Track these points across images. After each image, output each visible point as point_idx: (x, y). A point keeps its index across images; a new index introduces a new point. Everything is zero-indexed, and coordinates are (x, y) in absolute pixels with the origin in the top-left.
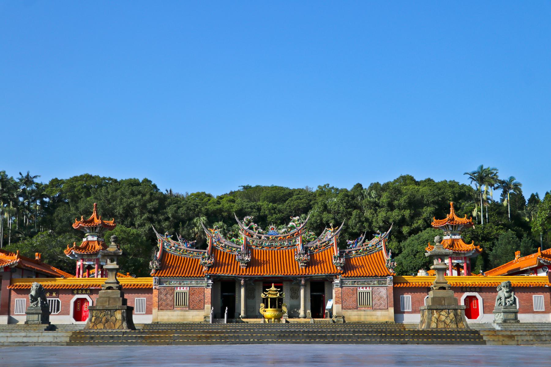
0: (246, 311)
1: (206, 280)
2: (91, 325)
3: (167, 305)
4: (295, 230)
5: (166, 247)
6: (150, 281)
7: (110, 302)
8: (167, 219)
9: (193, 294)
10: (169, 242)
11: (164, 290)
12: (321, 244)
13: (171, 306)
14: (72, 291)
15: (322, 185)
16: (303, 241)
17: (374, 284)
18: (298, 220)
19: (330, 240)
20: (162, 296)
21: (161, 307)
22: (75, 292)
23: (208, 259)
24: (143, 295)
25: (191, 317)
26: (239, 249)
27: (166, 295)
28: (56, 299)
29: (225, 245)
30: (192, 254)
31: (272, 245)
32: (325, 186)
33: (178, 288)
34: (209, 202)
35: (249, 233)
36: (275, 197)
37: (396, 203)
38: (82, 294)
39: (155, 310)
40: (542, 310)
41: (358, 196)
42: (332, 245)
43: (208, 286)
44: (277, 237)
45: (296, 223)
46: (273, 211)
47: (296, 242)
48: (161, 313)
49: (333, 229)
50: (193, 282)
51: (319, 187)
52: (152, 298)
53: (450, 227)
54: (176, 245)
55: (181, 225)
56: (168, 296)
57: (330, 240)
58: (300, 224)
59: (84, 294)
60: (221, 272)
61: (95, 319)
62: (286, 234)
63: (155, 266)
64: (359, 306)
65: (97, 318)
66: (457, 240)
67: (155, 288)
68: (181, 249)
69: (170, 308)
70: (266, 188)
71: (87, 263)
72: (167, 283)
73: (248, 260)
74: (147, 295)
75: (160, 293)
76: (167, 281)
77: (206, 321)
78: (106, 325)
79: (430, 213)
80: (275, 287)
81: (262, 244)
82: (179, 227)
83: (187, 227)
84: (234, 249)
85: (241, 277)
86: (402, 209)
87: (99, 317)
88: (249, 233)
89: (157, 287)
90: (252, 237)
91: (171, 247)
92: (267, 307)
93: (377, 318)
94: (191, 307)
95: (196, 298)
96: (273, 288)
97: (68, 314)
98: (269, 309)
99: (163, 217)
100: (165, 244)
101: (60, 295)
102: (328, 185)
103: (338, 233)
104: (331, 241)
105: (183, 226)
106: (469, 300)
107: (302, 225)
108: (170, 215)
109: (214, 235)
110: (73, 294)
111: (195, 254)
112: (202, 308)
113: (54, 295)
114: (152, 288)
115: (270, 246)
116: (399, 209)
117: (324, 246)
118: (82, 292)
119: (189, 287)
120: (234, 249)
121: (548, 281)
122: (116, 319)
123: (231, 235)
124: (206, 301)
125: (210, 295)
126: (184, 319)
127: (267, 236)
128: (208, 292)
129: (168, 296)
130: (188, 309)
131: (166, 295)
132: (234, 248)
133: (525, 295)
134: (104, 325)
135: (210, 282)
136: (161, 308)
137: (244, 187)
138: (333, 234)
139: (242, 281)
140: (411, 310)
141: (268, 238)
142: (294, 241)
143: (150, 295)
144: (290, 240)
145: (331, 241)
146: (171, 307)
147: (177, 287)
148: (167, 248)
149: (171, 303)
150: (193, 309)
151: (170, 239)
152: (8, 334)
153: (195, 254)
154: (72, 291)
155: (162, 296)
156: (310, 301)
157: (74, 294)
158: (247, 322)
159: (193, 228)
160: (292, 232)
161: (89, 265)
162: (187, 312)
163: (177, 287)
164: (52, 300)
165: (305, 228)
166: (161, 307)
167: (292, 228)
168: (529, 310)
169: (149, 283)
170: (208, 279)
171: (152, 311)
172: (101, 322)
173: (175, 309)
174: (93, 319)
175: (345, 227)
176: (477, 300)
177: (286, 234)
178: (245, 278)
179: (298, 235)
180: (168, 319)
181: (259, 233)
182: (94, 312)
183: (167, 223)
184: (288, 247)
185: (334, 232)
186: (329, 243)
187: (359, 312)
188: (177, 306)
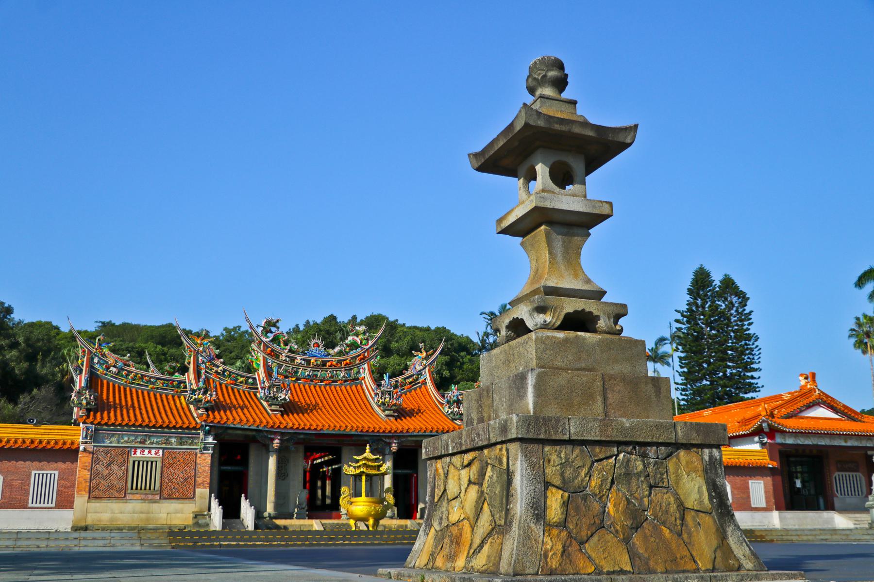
0: (277, 506)
1: (202, 435)
2: (552, 544)
3: (111, 487)
4: (359, 350)
5: (97, 366)
6: (77, 435)
7: (612, 398)
8: (14, 345)
9: (171, 465)
10: (104, 355)
11: (106, 454)
12: (405, 379)
13: (119, 491)
15: (231, 327)
16: (373, 371)
18: (364, 333)
19: (420, 373)
20: (100, 468)
21: (96, 493)
23: (205, 393)
25: (163, 516)
26: (250, 380)
27: (109, 465)
29: (224, 371)
30: (153, 383)
31: (316, 375)
32: (235, 328)
33: (139, 451)
34: (58, 337)
35: (272, 351)
36: (164, 337)
37: (394, 345)
39: (80, 501)
40: (50, 505)
41: (336, 332)
42: (424, 383)
43: (206, 449)
45: (361, 337)
46: (163, 357)
47: (359, 372)
48: (96, 505)
49: (424, 354)
50: (173, 440)
51: (226, 329)
52: (74, 472)
54: (120, 364)
55: (40, 357)
56: (115, 467)
57: (420, 373)
58: (367, 339)
60: (233, 419)
61: (566, 504)
62: (342, 358)
63: (84, 402)
64: (129, 491)
65: (575, 495)
67: (85, 450)
68: (130, 372)
69: (117, 495)
70: (146, 327)
72: (113, 439)
73: (285, 399)
74: (61, 465)
75: (95, 461)
76: (113, 435)
77: (197, 524)
78: (637, 539)
79: (442, 364)
80: (372, 452)
81: (297, 372)
82: (36, 360)
83: (50, 362)
84: (242, 379)
85: (275, 433)
86: (402, 357)
87: (580, 490)
88: (272, 351)
89: (90, 448)
90: (278, 357)
91: (108, 368)
92: (357, 494)
94: (165, 493)
95: (179, 474)
96: (368, 454)
98: (363, 498)
99: (7, 341)
100: (96, 360)
102: (240, 327)
103: (433, 361)
104: (421, 374)
105: (43, 360)
107: (370, 343)
108: (21, 340)
109: (201, 349)
111: (159, 384)
112: (189, 497)
114: (77, 450)
115: (311, 379)
116: (398, 354)
117: (411, 382)
119: (164, 449)
120: (242, 379)
121: (767, 458)
122: (683, 509)
123: (174, 368)
124: (199, 480)
125: (208, 469)
126: (148, 520)
127: (306, 357)
128: (205, 461)
130: (157, 497)
131: (109, 465)
132: (242, 376)
133: (738, 480)
134: (627, 540)
135: (210, 439)
136: (94, 494)
137: (103, 323)
138: (425, 362)
139: (277, 441)
141: (308, 362)
142: (355, 370)
143: (68, 465)
144: (349, 367)
145: (421, 374)
146: (121, 494)
148: (100, 370)
149: (120, 485)
150: (170, 498)
151: (106, 351)
153: (159, 384)
155: (100, 468)
158: (285, 528)
159: (61, 364)
160: (353, 353)
162: (155, 506)
163: (136, 448)
165: (377, 349)
166: (96, 493)
167: (353, 346)
169: (69, 439)
170: (207, 433)
171: (73, 502)
172: (600, 524)
173: (129, 497)
174: (555, 501)
177: (342, 358)
178: (282, 434)
179: (364, 360)
180: (111, 520)
181: (291, 351)
182: (555, 456)
183: (14, 353)
184: (346, 381)
185: (427, 358)
186: (417, 379)
188: (134, 491)
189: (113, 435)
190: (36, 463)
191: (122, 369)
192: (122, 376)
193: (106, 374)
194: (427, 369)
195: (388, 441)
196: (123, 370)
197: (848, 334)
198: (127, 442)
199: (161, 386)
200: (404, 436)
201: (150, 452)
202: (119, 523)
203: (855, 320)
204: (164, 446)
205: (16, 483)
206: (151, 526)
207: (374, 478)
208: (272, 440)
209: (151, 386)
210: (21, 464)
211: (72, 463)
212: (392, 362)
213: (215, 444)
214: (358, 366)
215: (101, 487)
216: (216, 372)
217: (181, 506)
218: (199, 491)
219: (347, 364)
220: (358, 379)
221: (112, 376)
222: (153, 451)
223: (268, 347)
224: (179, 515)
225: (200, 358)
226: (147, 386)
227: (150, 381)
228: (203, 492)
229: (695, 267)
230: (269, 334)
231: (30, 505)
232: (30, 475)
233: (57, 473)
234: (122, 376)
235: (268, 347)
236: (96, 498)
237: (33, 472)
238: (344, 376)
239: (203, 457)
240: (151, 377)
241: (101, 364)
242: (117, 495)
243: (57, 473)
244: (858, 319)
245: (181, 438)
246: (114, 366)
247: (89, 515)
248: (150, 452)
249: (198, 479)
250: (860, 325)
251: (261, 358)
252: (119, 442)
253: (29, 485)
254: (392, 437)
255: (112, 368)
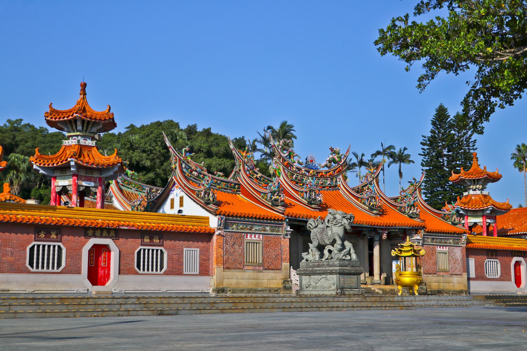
13: (240, 264)
14: (87, 231)
17: (450, 243)
22: (90, 232)
24: (196, 244)
25: (265, 281)
27: (233, 245)
28: (159, 248)
30: (219, 184)
33: (249, 235)
38: (101, 236)
39: (216, 270)
40: (195, 273)
43: (287, 235)
44: (318, 173)
47: (336, 181)
48: (228, 273)
53: (79, 123)
56: (236, 247)
59: (105, 237)
66: (89, 147)
71: (84, 184)
74: (201, 244)
93: (453, 286)
97: (510, 280)
100: (184, 166)
101: (65, 238)
106: (98, 251)
110: (87, 236)
113: (53, 236)
116: (217, 156)
118: (101, 234)
119: (263, 234)
126: (257, 284)
129: (236, 247)
130: (261, 268)
131: (233, 245)
139: (385, 235)
140: (198, 273)
144: (332, 177)
147: (247, 233)
151: (189, 159)
152: (427, 303)
154: (87, 231)
156: (368, 262)
157: (90, 237)
161: (86, 187)
162: (260, 274)
164: (44, 246)
168: (481, 276)
175: (170, 137)
176: (109, 251)
180: (237, 284)
184: (330, 187)
187: (438, 278)
189: (234, 223)
190: (186, 242)
191: (201, 173)
192: (200, 178)
193: (191, 177)
194: (375, 180)
195: (381, 231)
196: (201, 173)
197: (510, 156)
198: (242, 229)
199: (224, 187)
200: (390, 229)
201: (255, 236)
202: (241, 286)
203: (516, 147)
204: (262, 232)
205: (175, 257)
206: (259, 288)
207: (407, 258)
208: (383, 234)
209: (218, 186)
210: (177, 243)
211: (207, 243)
212: (214, 163)
213: (292, 232)
214: (336, 176)
215: (230, 261)
216: (256, 178)
217: (274, 274)
218: (284, 264)
219: (330, 175)
220: (336, 186)
221: (194, 178)
222: (257, 236)
223: (285, 161)
224: (274, 281)
225: (246, 167)
226: (215, 186)
227: (217, 183)
228: (286, 264)
229: (437, 106)
230: (285, 152)
231: (184, 273)
232: (183, 251)
233: (198, 249)
234: (200, 178)
235: (285, 161)
236: (228, 268)
237: (185, 249)
238: (329, 184)
239: (285, 240)
240: (218, 180)
241: (187, 169)
242: (239, 266)
243: (198, 249)
244: (518, 146)
245: (433, 239)
246: (196, 171)
247: (224, 280)
248: (255, 236)
249: (283, 256)
250: (519, 150)
251: (281, 168)
252: (237, 229)
253: (182, 258)
254: (384, 229)
255: (194, 172)
